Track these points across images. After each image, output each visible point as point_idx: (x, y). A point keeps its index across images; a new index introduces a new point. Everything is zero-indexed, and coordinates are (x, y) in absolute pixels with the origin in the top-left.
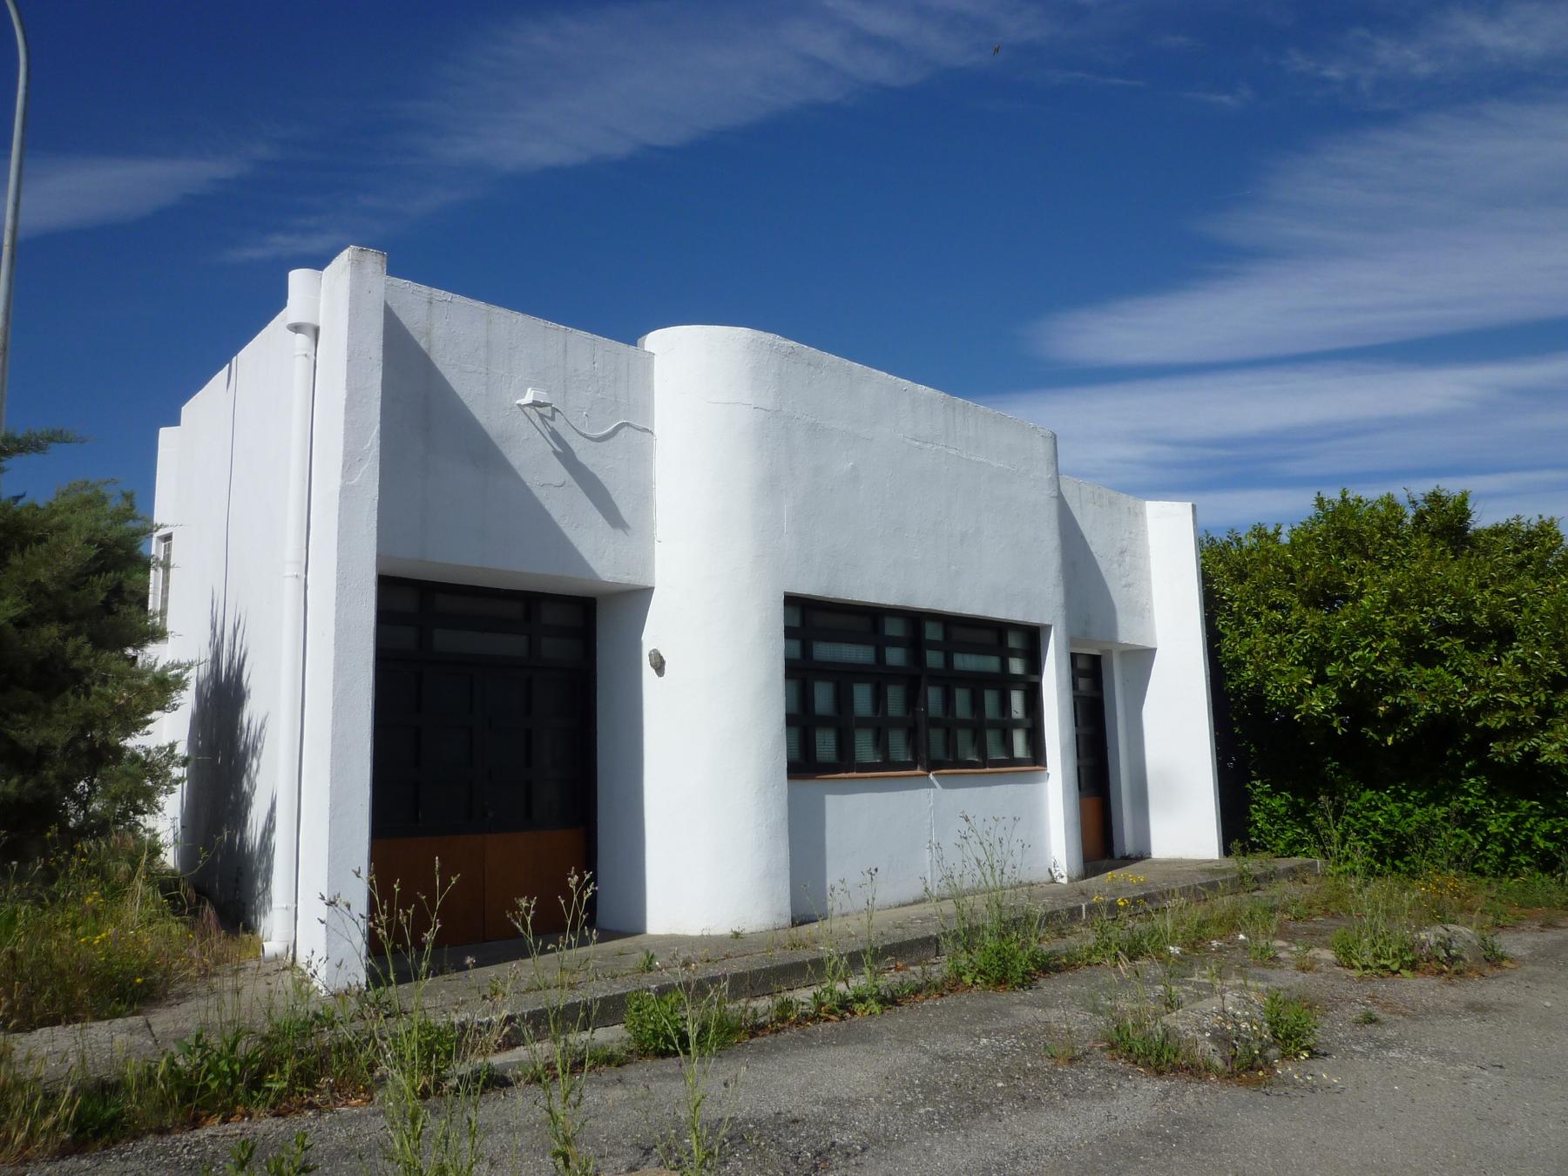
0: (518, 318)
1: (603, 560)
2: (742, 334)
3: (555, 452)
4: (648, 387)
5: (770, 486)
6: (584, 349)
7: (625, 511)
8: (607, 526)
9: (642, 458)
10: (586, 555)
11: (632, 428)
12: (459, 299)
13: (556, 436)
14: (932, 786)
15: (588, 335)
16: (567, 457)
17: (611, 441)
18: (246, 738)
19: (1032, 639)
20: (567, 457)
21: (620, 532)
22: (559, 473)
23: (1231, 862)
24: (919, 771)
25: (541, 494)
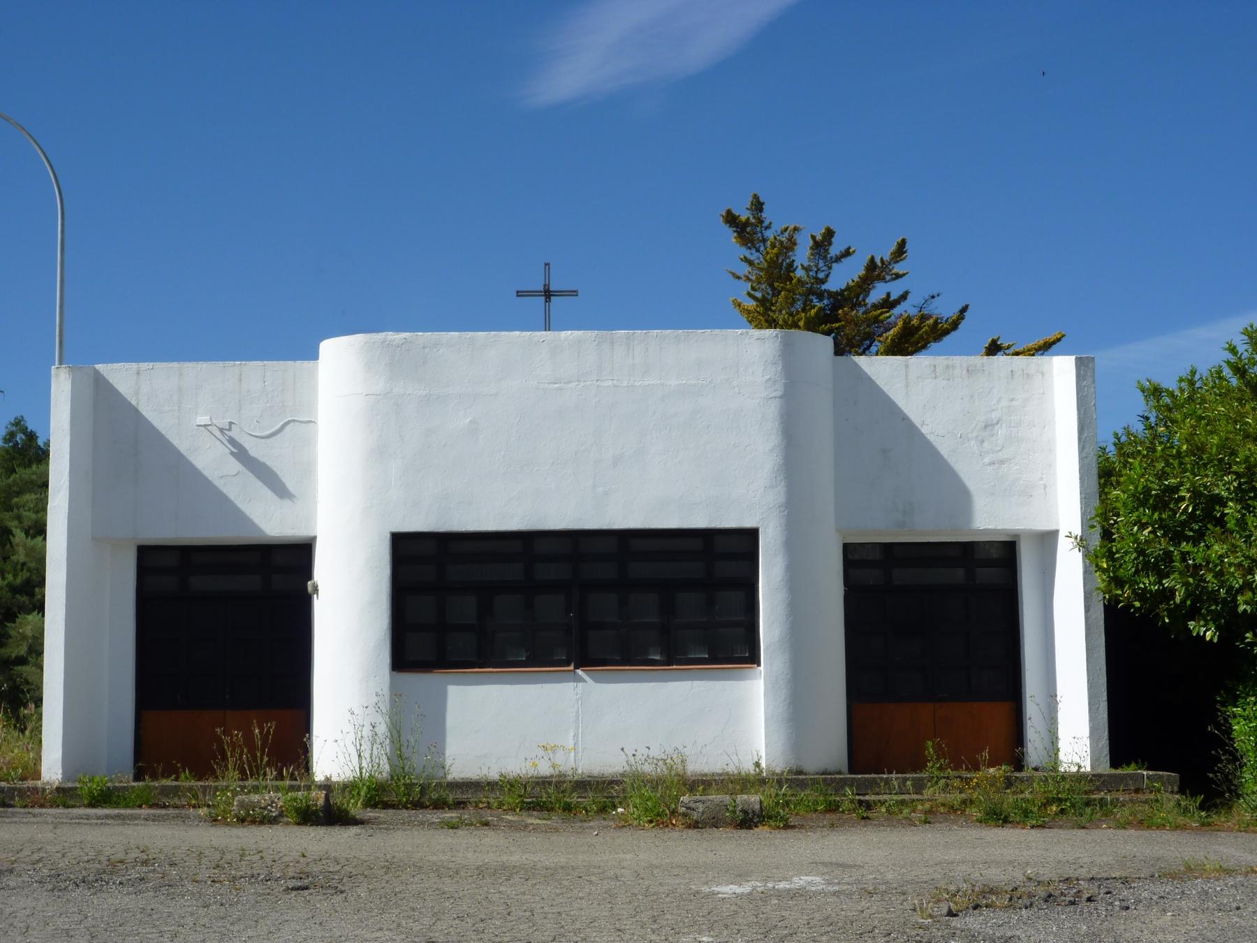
0: (204, 366)
1: (272, 522)
2: (359, 339)
3: (232, 453)
4: (314, 388)
5: (379, 453)
6: (256, 375)
7: (290, 485)
8: (275, 497)
9: (308, 443)
10: (256, 521)
11: (295, 422)
12: (158, 365)
13: (232, 441)
14: (581, 680)
15: (260, 363)
16: (241, 454)
17: (278, 436)
18: (662, 770)
19: (743, 544)
20: (241, 454)
21: (287, 502)
22: (235, 466)
23: (1113, 771)
24: (572, 668)
25: (218, 483)
